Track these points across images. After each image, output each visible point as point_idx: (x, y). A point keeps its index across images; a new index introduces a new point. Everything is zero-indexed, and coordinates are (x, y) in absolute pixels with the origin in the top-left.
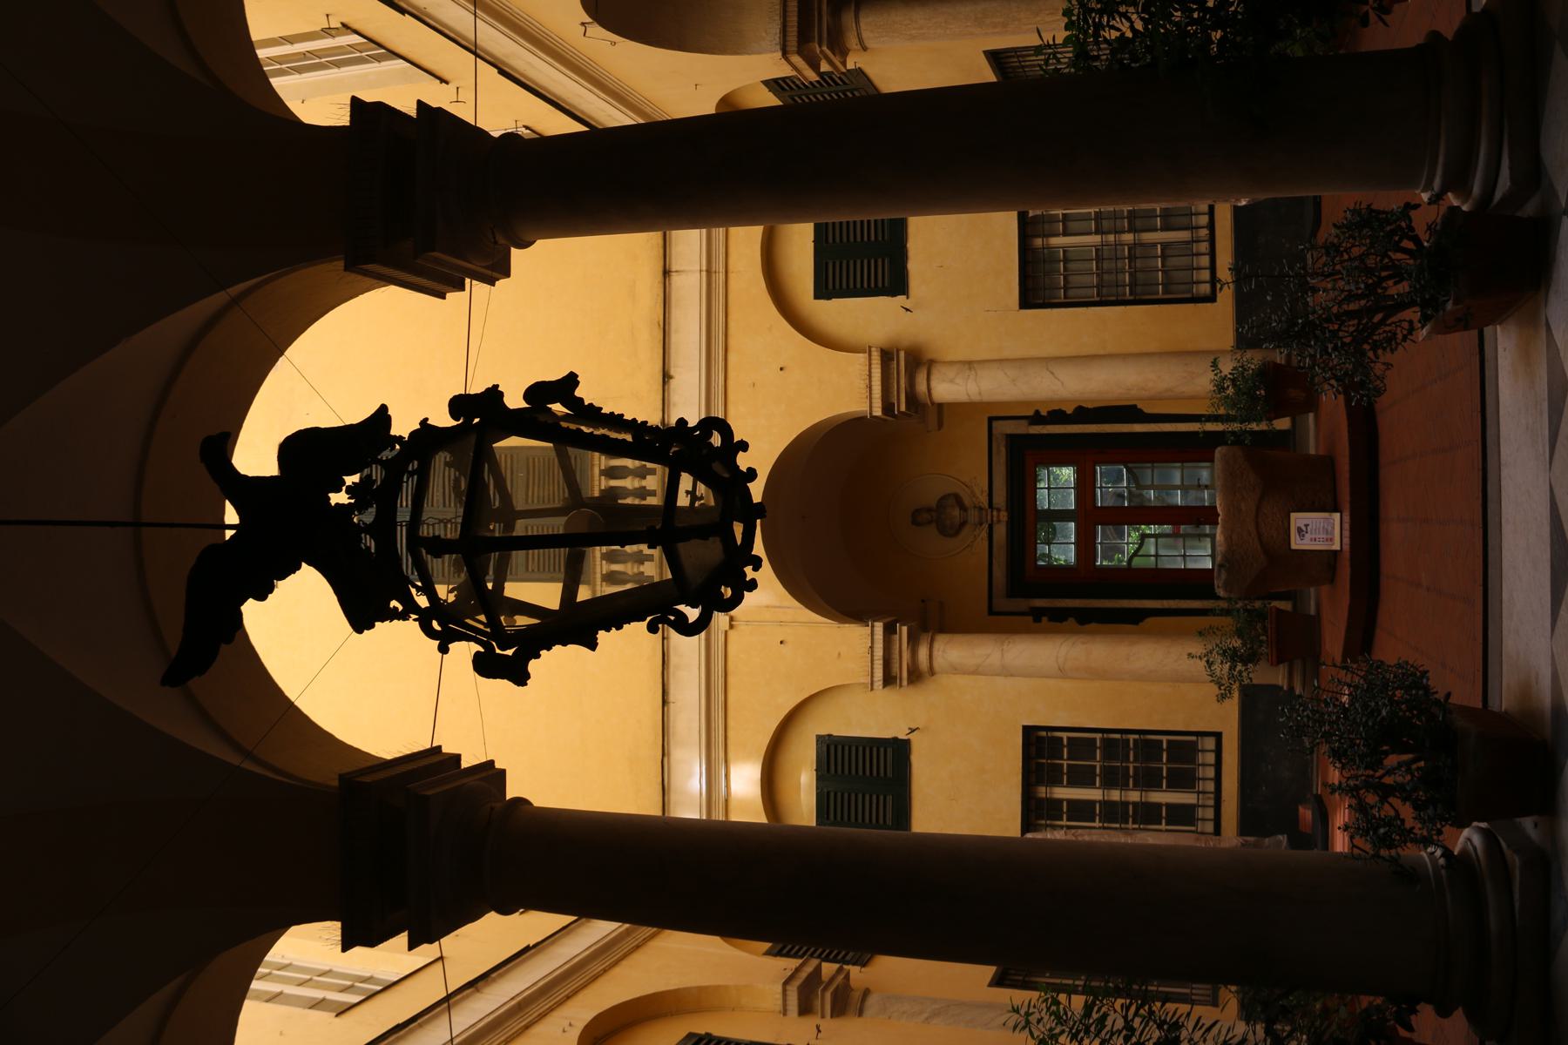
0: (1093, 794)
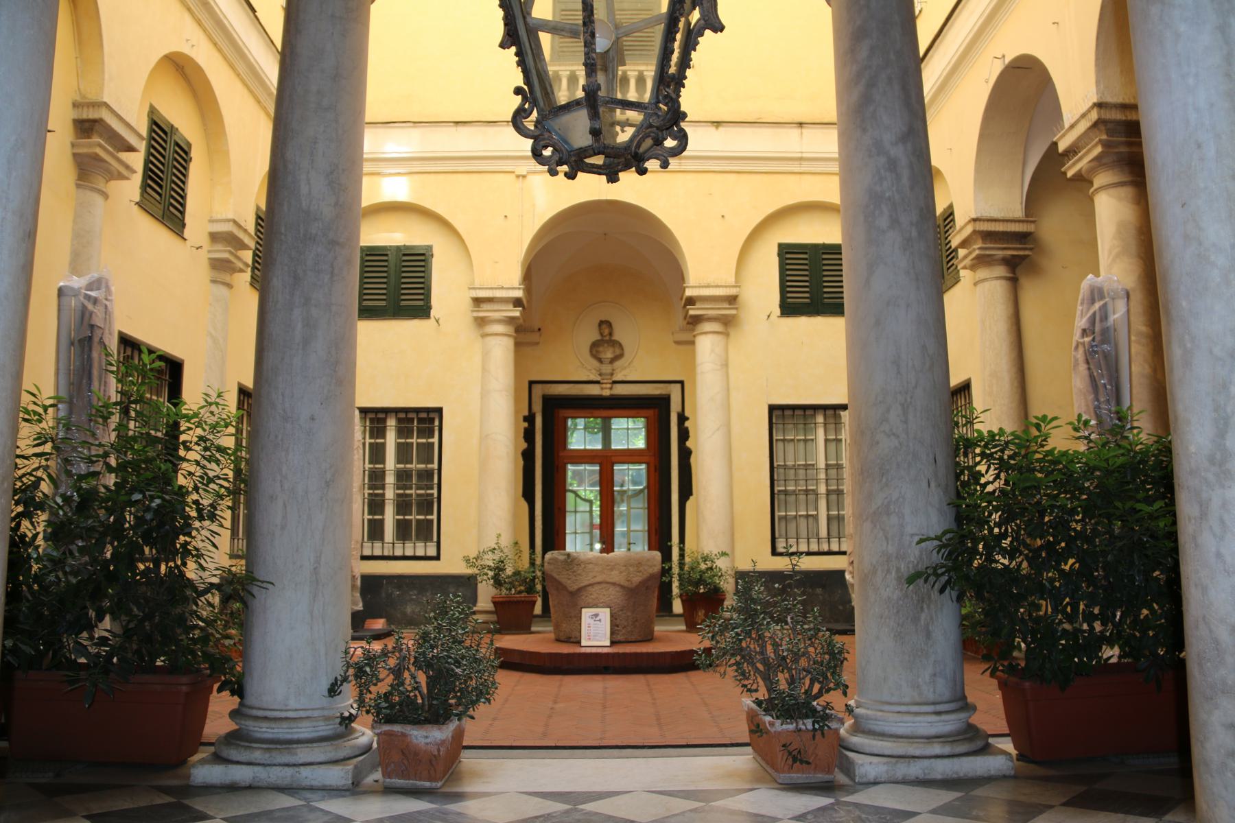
0: (391, 462)
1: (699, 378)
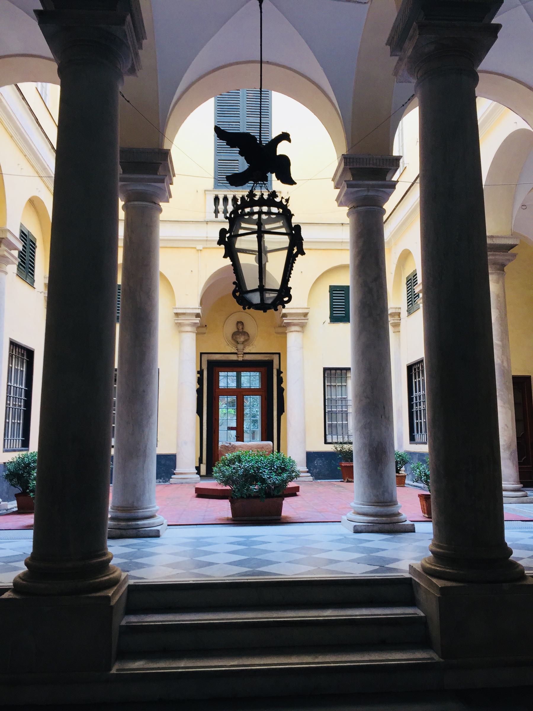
1: (289, 350)
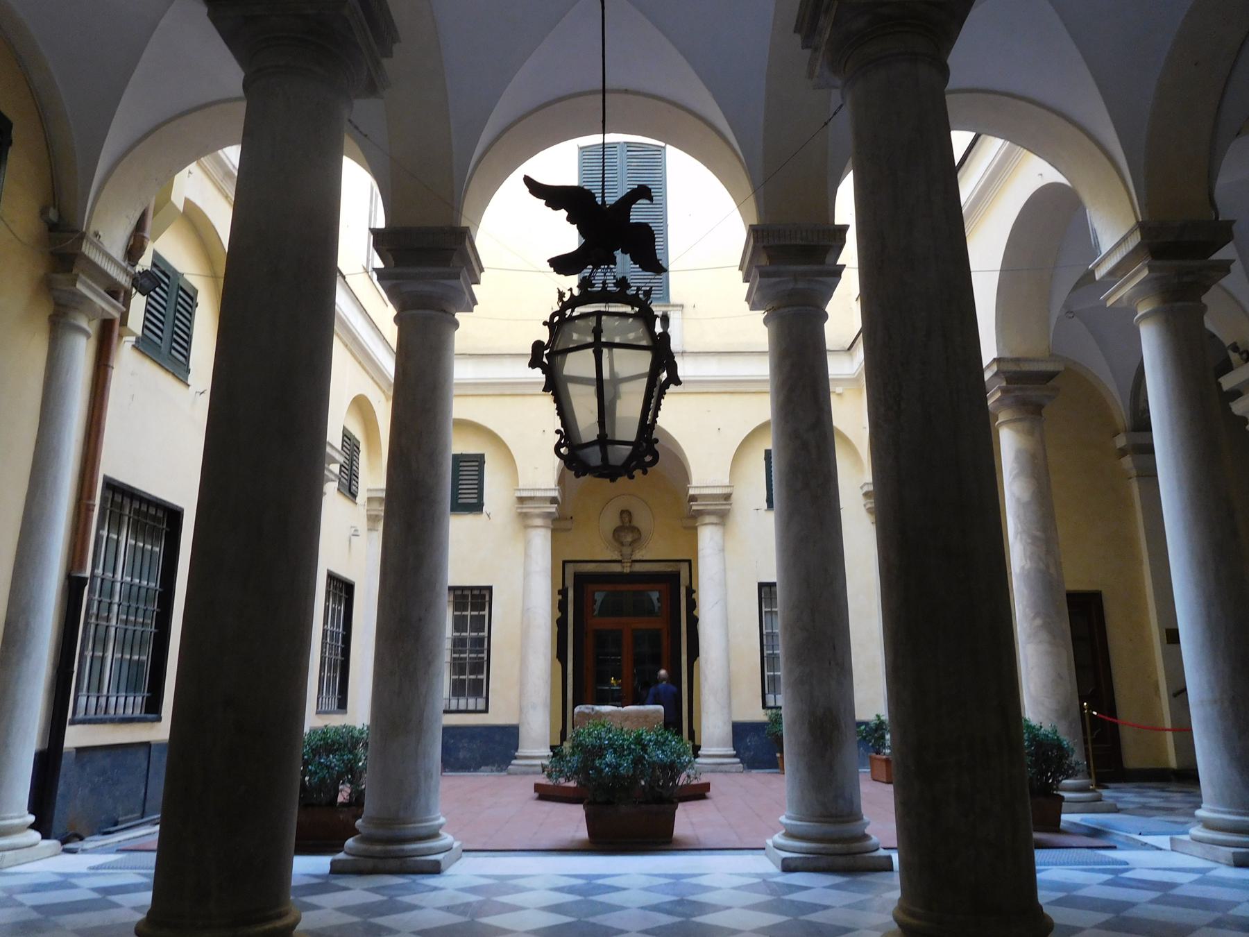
1: (700, 554)
